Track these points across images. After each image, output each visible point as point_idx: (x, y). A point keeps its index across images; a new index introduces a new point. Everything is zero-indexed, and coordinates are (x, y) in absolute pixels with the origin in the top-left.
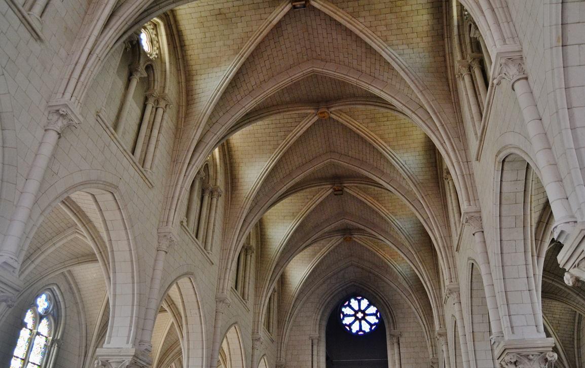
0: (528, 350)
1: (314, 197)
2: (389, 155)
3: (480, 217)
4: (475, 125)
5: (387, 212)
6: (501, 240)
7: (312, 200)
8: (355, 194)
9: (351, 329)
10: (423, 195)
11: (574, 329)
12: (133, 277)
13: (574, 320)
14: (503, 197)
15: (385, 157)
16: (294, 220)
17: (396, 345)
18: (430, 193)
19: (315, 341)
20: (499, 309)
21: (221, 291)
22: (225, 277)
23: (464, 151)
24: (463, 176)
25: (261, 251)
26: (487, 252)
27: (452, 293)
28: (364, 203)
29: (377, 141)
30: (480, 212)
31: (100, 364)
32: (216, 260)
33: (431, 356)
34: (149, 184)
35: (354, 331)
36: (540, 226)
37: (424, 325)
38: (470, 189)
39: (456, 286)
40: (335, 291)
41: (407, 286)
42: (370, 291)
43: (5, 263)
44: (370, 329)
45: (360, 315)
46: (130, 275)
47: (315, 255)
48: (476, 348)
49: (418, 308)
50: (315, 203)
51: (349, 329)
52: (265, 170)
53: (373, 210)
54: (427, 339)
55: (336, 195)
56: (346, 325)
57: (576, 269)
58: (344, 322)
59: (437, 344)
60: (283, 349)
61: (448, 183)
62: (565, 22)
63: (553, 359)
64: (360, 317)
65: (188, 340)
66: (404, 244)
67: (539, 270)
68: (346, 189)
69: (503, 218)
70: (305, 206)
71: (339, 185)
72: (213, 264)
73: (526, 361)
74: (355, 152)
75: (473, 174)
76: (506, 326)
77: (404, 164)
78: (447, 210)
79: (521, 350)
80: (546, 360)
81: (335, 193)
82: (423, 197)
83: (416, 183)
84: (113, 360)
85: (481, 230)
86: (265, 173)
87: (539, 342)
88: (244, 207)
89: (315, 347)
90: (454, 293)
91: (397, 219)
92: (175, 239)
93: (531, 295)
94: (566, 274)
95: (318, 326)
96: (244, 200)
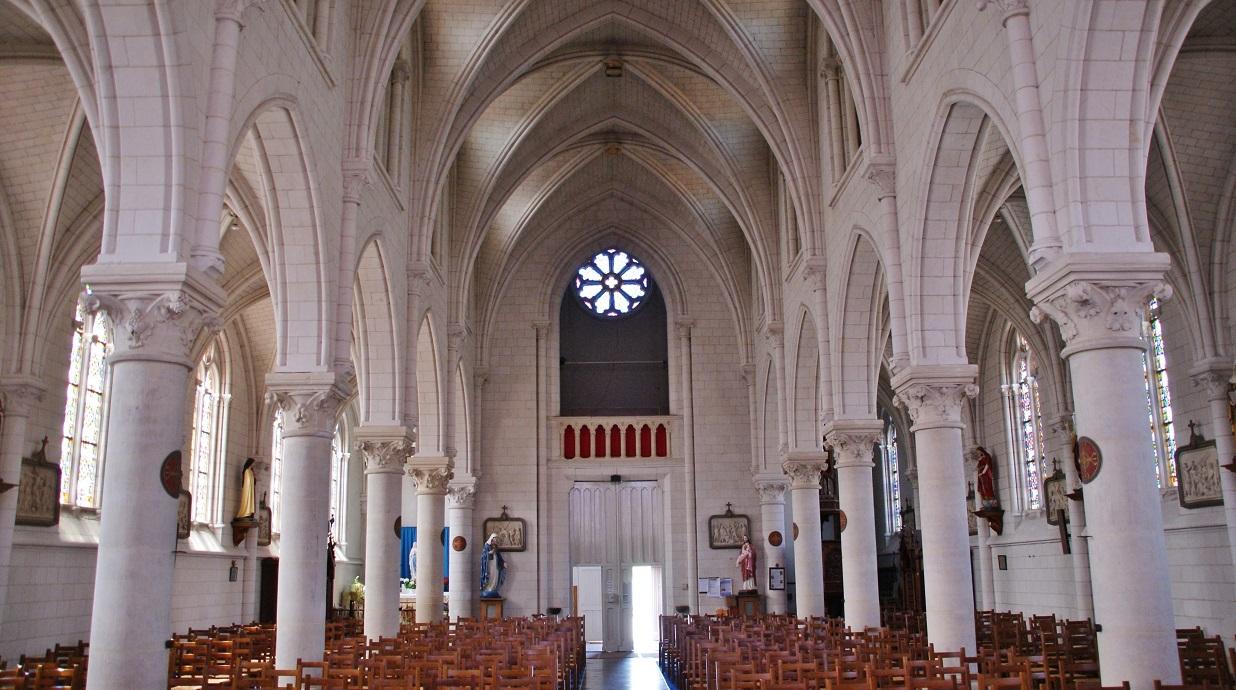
0: (942, 380)
1: (564, 75)
2: (728, 21)
3: (894, 173)
4: (907, 19)
5: (698, 112)
6: (926, 219)
7: (561, 82)
8: (643, 77)
9: (594, 307)
10: (780, 101)
11: (982, 331)
12: (317, 254)
13: (985, 317)
14: (941, 153)
15: (721, 29)
16: (525, 118)
17: (684, 341)
18: (791, 96)
19: (543, 332)
20: (908, 320)
21: (415, 256)
22: (420, 231)
23: (878, 55)
24: (873, 99)
25: (458, 172)
26: (898, 231)
27: (813, 273)
28: (656, 92)
29: (736, 28)
30: (895, 164)
31: (275, 398)
32: (405, 205)
33: (743, 362)
34: (328, 81)
35: (600, 310)
36: (983, 198)
37: (735, 308)
38: (882, 124)
39: (822, 263)
40: (580, 243)
41: (712, 242)
42: (643, 244)
43: (212, 268)
44: (630, 307)
45: (612, 282)
46: (311, 250)
47: (548, 177)
48: (846, 363)
49: (727, 279)
50: (566, 87)
51: (590, 307)
52: (493, 32)
53: (672, 106)
54: (738, 331)
55: (609, 76)
56: (586, 299)
57: (1048, 304)
58: (583, 294)
59: (756, 342)
60: (486, 344)
61: (827, 84)
62: (1137, 88)
63: (973, 393)
64: (612, 286)
65: (367, 345)
66: (722, 171)
67: (971, 265)
68: (628, 66)
69: (934, 187)
70: (547, 91)
71: (616, 57)
72: (402, 209)
73: (937, 395)
74: (661, 7)
75: (889, 98)
76: (915, 345)
77: (751, 39)
78: (818, 132)
79: (931, 381)
80: (964, 394)
81: (609, 72)
82: (778, 104)
83: (770, 79)
84: (297, 392)
85: (890, 194)
86: (493, 36)
87: (959, 370)
88: (452, 101)
89: (542, 342)
90: (817, 274)
91: (715, 127)
92: (370, 181)
93: (955, 303)
94: (1034, 308)
95: (547, 306)
96: (452, 88)
